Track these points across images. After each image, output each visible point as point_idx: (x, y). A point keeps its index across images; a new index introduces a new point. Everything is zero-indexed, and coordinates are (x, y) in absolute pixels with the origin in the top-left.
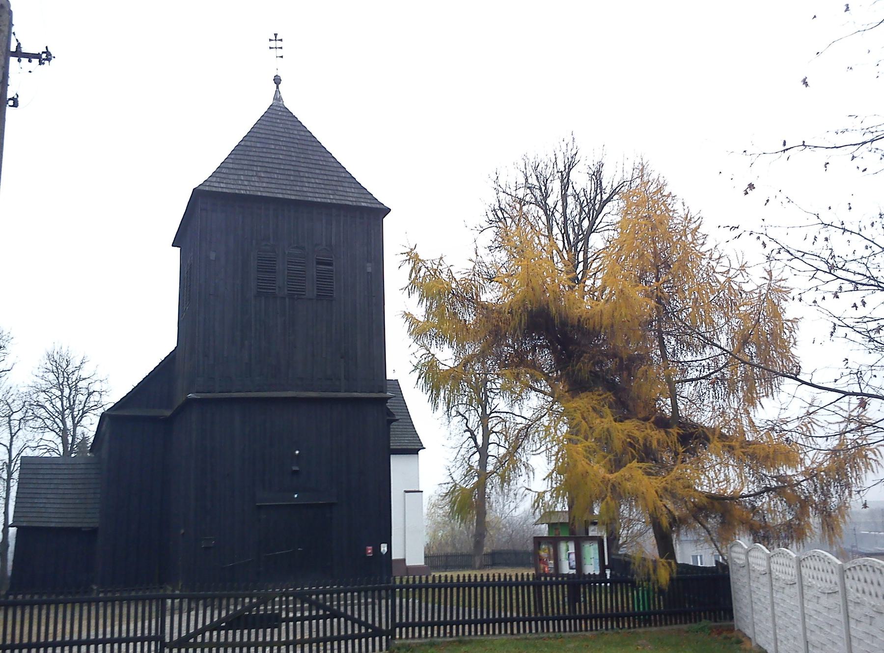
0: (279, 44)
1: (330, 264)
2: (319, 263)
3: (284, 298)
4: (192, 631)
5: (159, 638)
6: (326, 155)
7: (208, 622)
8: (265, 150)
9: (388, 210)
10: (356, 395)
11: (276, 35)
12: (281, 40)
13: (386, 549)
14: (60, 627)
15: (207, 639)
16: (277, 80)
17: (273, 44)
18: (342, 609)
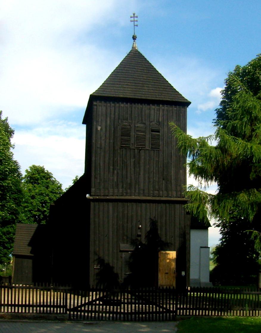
0: (136, 19)
1: (159, 132)
2: (153, 131)
3: (135, 149)
4: (79, 304)
5: (65, 306)
6: (178, 96)
7: (87, 301)
8: (127, 74)
9: (188, 103)
10: (172, 199)
11: (134, 14)
12: (137, 17)
13: (184, 274)
14: (52, 300)
15: (86, 309)
16: (134, 38)
17: (132, 19)
18: (154, 301)
